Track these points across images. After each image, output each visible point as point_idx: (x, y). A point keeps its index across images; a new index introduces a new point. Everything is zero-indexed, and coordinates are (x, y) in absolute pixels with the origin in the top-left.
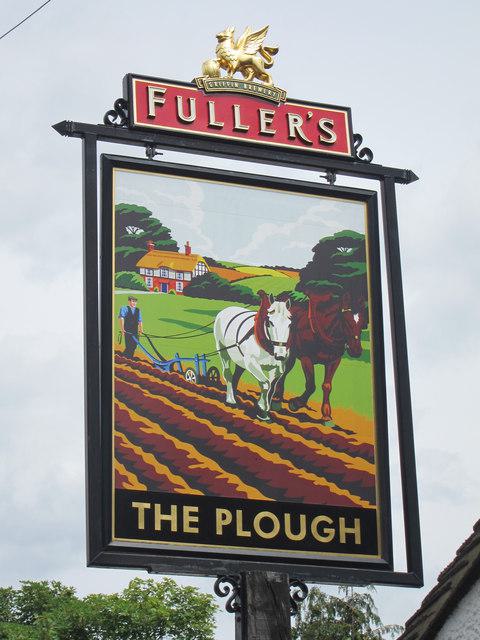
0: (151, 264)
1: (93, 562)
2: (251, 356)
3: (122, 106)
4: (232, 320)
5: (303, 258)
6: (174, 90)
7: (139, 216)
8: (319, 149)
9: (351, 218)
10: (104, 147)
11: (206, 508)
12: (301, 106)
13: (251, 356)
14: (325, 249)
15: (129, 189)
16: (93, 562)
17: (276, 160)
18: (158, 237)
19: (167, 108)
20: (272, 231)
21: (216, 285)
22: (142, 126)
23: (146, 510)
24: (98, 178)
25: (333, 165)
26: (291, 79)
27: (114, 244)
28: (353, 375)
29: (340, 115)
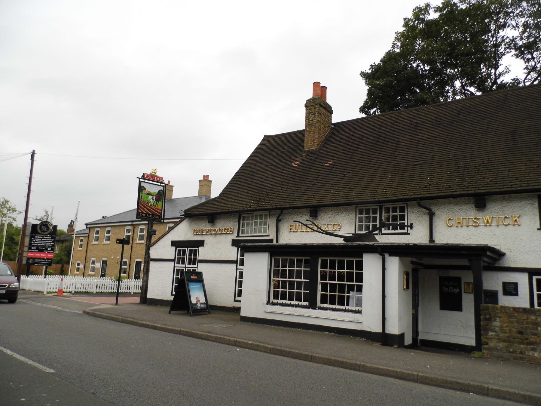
0: (144, 191)
1: (516, 294)
2: (151, 201)
3: (143, 176)
4: (150, 197)
5: (157, 192)
6: (148, 175)
7: (143, 187)
8: (160, 180)
9: (162, 188)
10: (141, 180)
11: (146, 214)
12: (159, 177)
13: (151, 201)
14: (159, 191)
15: (143, 184)
16: (516, 294)
17: (91, 224)
18: (145, 189)
19: (147, 177)
20: (154, 189)
21: (149, 194)
22: (145, 177)
23: (404, 223)
24: (140, 183)
25: (161, 183)
26: (159, 174)
27: (141, 189)
28: (160, 203)
29: (162, 178)
